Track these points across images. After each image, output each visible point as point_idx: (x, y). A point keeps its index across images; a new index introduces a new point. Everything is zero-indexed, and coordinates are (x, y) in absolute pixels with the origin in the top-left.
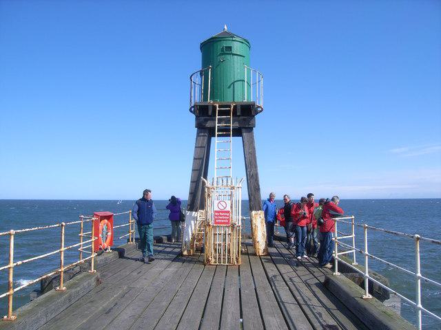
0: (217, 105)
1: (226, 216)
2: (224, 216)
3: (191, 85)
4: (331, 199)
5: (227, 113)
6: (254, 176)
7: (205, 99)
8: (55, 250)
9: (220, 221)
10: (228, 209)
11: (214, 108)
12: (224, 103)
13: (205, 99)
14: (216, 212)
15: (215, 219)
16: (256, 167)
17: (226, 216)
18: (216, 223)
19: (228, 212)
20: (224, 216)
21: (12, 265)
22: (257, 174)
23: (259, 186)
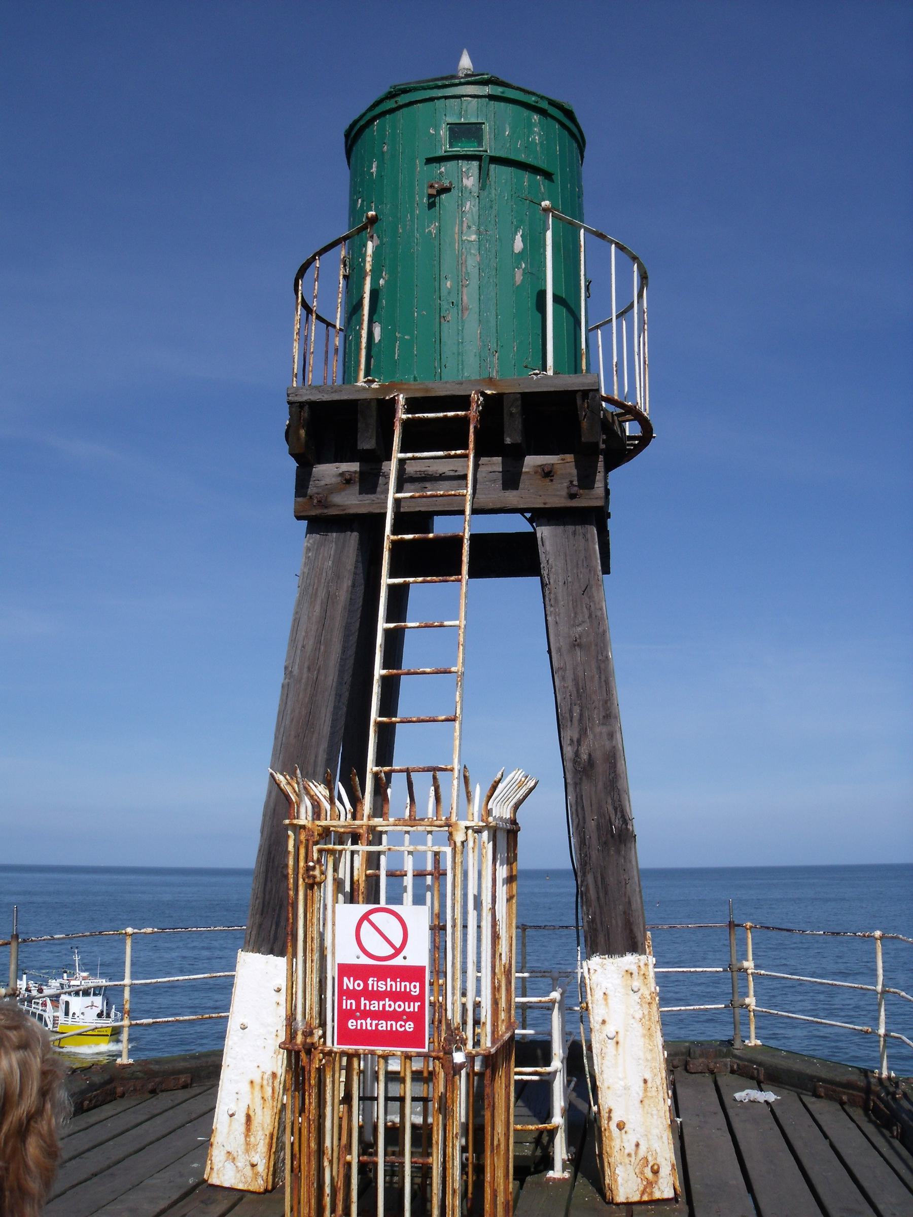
0: (401, 399)
1: (405, 997)
2: (395, 996)
3: (533, 94)
4: (636, 997)
5: (447, 436)
6: (601, 767)
7: (349, 374)
8: (457, 657)
9: (369, 1024)
10: (418, 954)
11: (387, 408)
12: (441, 390)
13: (349, 374)
14: (346, 970)
15: (345, 1015)
16: (609, 716)
17: (405, 997)
18: (345, 1036)
19: (415, 973)
20: (395, 996)
21: (127, 981)
22: (613, 758)
23: (625, 820)
